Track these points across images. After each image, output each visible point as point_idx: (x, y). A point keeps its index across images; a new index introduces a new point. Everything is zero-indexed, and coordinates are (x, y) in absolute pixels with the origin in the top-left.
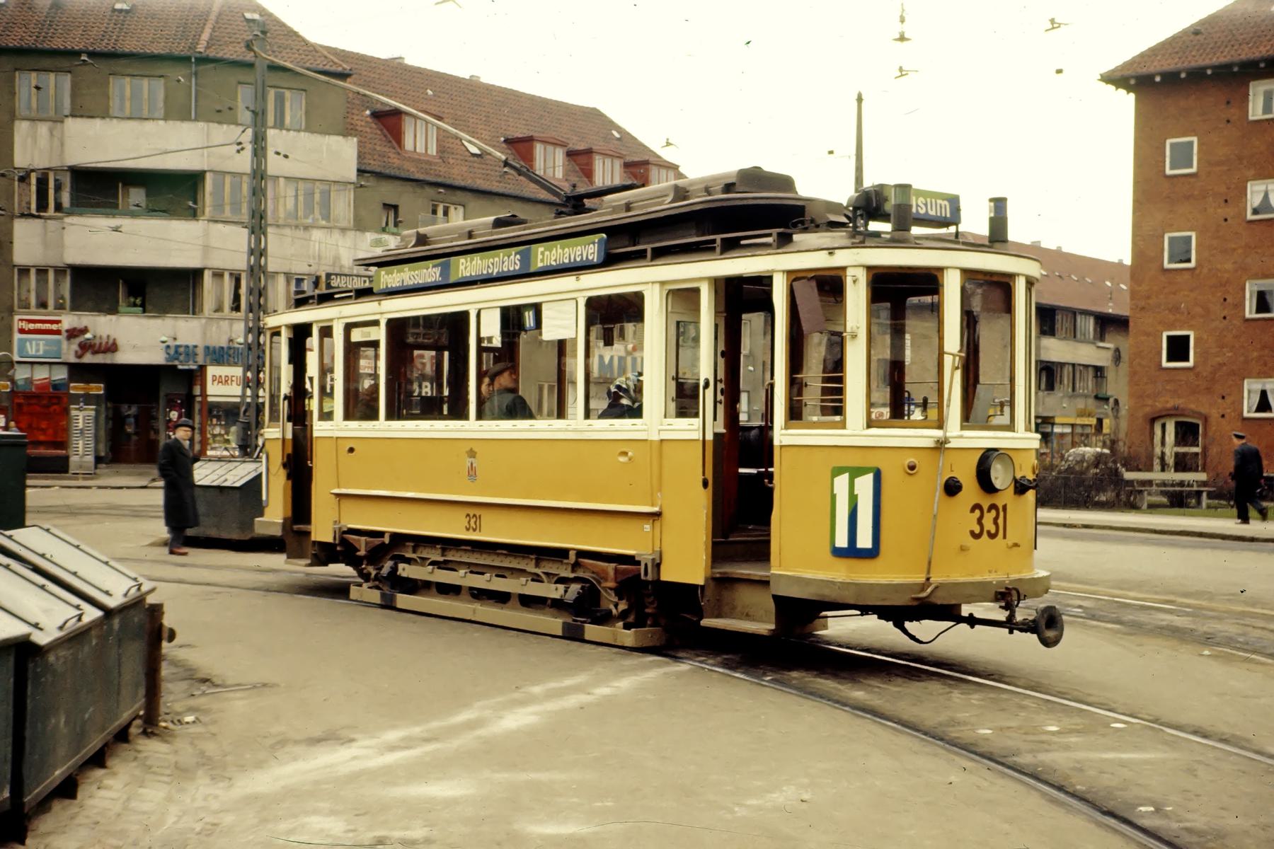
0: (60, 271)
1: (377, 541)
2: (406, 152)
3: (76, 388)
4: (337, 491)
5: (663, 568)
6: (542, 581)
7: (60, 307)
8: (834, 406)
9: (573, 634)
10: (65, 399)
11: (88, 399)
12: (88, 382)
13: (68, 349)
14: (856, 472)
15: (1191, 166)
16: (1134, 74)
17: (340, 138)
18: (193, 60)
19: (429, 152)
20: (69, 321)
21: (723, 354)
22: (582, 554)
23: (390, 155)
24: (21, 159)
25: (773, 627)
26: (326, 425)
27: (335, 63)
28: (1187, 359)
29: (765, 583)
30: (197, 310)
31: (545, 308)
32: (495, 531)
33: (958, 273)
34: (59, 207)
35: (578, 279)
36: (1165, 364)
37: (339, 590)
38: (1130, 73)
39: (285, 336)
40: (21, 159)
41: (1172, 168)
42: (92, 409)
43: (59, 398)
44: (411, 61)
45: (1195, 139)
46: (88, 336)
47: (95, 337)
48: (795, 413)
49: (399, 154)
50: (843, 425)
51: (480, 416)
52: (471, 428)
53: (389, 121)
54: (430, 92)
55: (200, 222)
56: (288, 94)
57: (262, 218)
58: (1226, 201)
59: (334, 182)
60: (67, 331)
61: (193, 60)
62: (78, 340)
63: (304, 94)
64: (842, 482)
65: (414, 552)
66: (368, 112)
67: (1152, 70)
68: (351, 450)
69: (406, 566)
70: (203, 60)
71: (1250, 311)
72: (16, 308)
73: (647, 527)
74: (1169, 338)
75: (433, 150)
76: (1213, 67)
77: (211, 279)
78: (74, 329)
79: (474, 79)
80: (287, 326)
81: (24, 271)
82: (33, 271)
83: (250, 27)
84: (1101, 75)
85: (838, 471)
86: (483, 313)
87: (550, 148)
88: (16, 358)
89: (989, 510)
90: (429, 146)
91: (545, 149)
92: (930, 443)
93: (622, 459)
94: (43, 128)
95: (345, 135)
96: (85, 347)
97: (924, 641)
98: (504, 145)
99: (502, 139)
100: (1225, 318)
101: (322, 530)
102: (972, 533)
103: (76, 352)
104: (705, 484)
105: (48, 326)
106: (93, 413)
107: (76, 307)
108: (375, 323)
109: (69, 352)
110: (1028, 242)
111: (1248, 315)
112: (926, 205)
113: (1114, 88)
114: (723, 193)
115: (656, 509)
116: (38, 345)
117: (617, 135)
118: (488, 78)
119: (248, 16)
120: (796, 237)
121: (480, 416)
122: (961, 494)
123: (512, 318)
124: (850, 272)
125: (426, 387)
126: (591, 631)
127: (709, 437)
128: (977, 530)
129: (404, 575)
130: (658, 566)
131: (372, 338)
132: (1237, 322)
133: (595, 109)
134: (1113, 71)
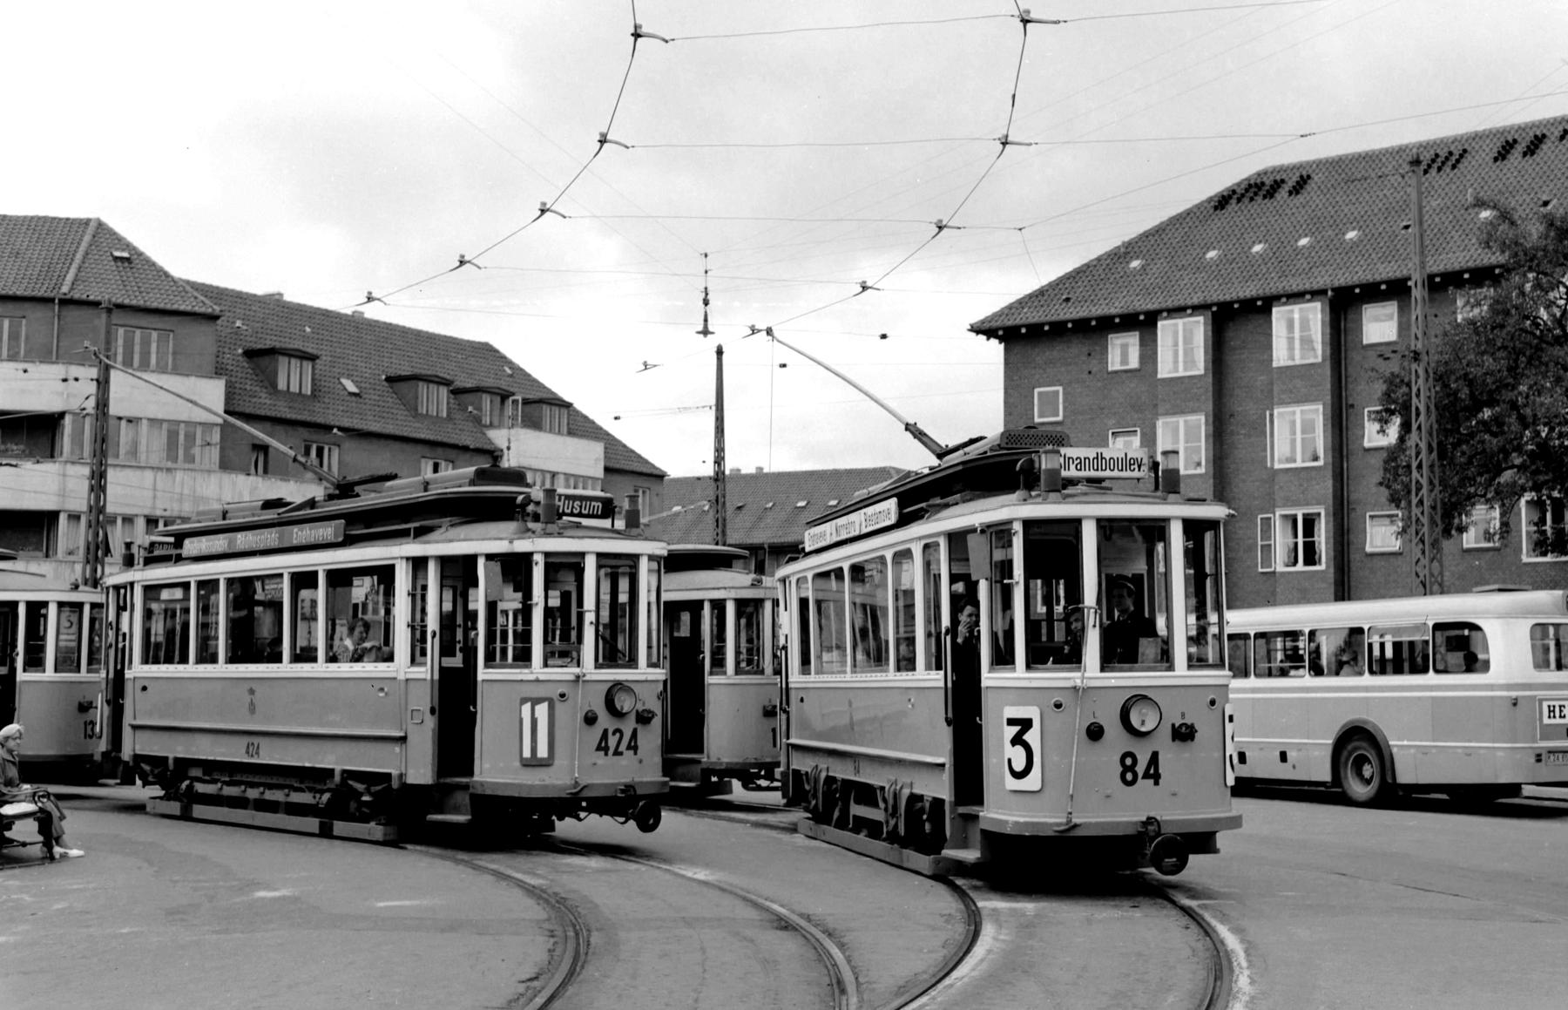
8: (524, 657)
9: (326, 833)
14: (536, 702)
18: (57, 301)
23: (261, 394)
25: (469, 817)
29: (466, 787)
30: (51, 553)
32: (271, 755)
38: (999, 324)
41: (1041, 416)
44: (292, 296)
45: (1060, 389)
48: (490, 659)
54: (308, 330)
55: (57, 464)
56: (155, 335)
61: (57, 301)
63: (171, 335)
64: (526, 708)
70: (66, 302)
73: (397, 749)
76: (1074, 321)
77: (66, 522)
85: (524, 701)
89: (614, 734)
92: (572, 678)
93: (382, 694)
98: (385, 383)
104: (433, 711)
112: (581, 507)
113: (984, 337)
114: (470, 485)
115: (402, 734)
119: (117, 254)
125: (1463, 453)
126: (339, 827)
129: (200, 791)
134: (983, 322)
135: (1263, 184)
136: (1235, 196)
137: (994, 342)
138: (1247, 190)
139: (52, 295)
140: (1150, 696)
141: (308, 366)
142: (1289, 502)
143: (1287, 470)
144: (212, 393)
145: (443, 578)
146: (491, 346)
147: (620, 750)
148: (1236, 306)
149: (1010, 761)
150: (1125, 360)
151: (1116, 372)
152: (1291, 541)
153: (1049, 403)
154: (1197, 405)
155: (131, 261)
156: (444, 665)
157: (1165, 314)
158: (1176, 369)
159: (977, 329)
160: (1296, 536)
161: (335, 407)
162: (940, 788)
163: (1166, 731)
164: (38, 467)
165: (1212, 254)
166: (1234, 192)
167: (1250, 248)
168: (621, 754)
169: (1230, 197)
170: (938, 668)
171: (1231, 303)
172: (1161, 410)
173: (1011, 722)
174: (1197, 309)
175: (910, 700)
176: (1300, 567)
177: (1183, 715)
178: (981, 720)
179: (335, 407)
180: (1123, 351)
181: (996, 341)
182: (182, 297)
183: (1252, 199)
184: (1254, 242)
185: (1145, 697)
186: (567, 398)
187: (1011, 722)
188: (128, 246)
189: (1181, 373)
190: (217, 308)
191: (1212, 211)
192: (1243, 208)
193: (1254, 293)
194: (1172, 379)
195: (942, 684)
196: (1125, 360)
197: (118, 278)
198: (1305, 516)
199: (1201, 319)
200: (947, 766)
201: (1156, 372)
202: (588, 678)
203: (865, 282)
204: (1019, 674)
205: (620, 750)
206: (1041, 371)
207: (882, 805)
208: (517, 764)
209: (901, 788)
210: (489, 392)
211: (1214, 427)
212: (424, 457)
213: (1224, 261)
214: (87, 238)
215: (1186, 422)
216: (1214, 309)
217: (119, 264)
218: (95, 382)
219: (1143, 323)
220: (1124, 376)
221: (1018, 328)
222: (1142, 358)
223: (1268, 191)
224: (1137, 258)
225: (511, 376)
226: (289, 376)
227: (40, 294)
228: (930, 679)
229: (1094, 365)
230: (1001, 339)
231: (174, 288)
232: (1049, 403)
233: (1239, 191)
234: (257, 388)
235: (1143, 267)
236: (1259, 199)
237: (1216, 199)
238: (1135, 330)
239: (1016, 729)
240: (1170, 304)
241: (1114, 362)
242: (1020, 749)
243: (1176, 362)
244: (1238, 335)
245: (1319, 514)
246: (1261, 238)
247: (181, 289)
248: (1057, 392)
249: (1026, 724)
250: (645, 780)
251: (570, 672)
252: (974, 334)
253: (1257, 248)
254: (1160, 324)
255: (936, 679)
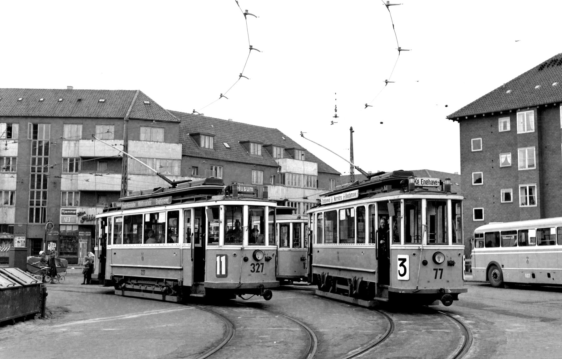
0: (77, 193)
1: (121, 278)
2: (202, 148)
3: (81, 234)
4: (111, 265)
5: (184, 282)
6: (158, 287)
7: (76, 205)
10: (77, 237)
11: (84, 237)
12: (85, 231)
13: (78, 220)
15: (480, 149)
16: (458, 116)
17: (176, 144)
19: (210, 148)
20: (79, 210)
21: (201, 226)
22: (166, 280)
24: (65, 154)
26: (109, 246)
27: (175, 118)
28: (482, 218)
31: (160, 214)
32: (148, 275)
33: (247, 206)
34: (77, 170)
35: (166, 207)
36: (474, 220)
37: (112, 293)
39: (100, 220)
40: (65, 154)
41: (474, 149)
42: (86, 241)
43: (75, 237)
45: (481, 139)
46: (85, 215)
47: (87, 215)
49: (199, 149)
50: (218, 244)
51: (115, 243)
52: (142, 246)
53: (196, 137)
54: (212, 126)
57: (125, 179)
58: (492, 161)
59: (174, 160)
60: (78, 213)
62: (81, 217)
64: (218, 258)
65: (130, 281)
66: (188, 134)
67: (464, 115)
68: (115, 254)
69: (128, 285)
71: (502, 200)
72: (61, 206)
74: (475, 210)
75: (212, 147)
78: (81, 213)
79: (230, 120)
80: (101, 218)
81: (64, 193)
82: (67, 193)
83: (146, 106)
84: (447, 117)
85: (217, 256)
86: (146, 215)
87: (256, 145)
88: (61, 223)
89: (256, 265)
90: (210, 145)
91: (254, 145)
92: (240, 249)
93: (175, 255)
94: (72, 143)
95: (177, 143)
96: (84, 219)
97: (245, 298)
99: (239, 142)
100: (494, 203)
101: (108, 277)
102: (251, 271)
103: (81, 221)
104: (192, 260)
105: (72, 212)
106: (87, 242)
107: (82, 205)
108: (121, 217)
109: (78, 221)
110: (453, 173)
111: (502, 202)
112: (246, 189)
113: (452, 121)
116: (68, 219)
117: (284, 138)
118: (235, 120)
119: (145, 102)
120: (212, 197)
121: (325, 242)
122: (535, 275)
123: (152, 216)
124: (221, 206)
127: (193, 248)
128: (253, 270)
130: (182, 282)
131: (121, 221)
132: (498, 204)
133: (276, 129)
134: (451, 115)
135: (557, 60)
136: (546, 65)
137: (456, 122)
138: (551, 63)
139: (123, 117)
140: (442, 252)
141: (211, 138)
142: (523, 182)
143: (523, 171)
144: (176, 150)
145: (196, 215)
146: (278, 130)
147: (259, 270)
148: (546, 106)
149: (399, 271)
150: (505, 127)
151: (502, 132)
152: (524, 196)
153: (477, 145)
154: (532, 143)
155: (151, 105)
156: (195, 246)
157: (519, 110)
158: (524, 130)
159: (449, 118)
160: (526, 194)
161: (221, 153)
162: (374, 279)
163: (446, 263)
164: (108, 175)
165: (537, 87)
166: (546, 63)
167: (552, 84)
168: (259, 272)
169: (545, 65)
170: (373, 242)
171: (544, 105)
172: (519, 145)
173: (400, 259)
174: (531, 108)
175: (363, 252)
176: (528, 205)
177: (451, 258)
178: (389, 258)
179: (221, 153)
180: (504, 124)
181: (457, 122)
182: (167, 116)
183: (553, 66)
184: (553, 82)
185: (440, 252)
186: (305, 148)
187: (400, 259)
188: (149, 99)
189: (526, 132)
190: (179, 119)
191: (538, 70)
192: (549, 69)
193: (553, 101)
194: (523, 134)
195: (375, 248)
196: (505, 127)
197: (146, 110)
198: (529, 187)
199: (533, 111)
200: (376, 273)
201: (516, 131)
202: (245, 249)
203: (367, 104)
204: (402, 245)
205: (259, 270)
206: (474, 132)
207: (349, 285)
208: (216, 277)
209: (358, 279)
210: (275, 146)
211: (539, 151)
212: (253, 170)
213: (542, 89)
214: (136, 97)
215: (528, 150)
216: (538, 107)
217: (146, 105)
218: (123, 146)
219: (511, 113)
220: (505, 133)
221: (464, 117)
222: (511, 126)
223: (559, 62)
224: (509, 89)
225: (284, 140)
226: (205, 142)
227: (119, 117)
228: (369, 246)
229: (493, 129)
230: (459, 121)
231: (165, 113)
232: (477, 145)
233: (548, 63)
234: (195, 147)
235: (511, 93)
236: (556, 66)
237: (540, 66)
238: (508, 116)
239: (401, 262)
240: (521, 106)
241: (501, 129)
242: (402, 268)
243: (524, 128)
244: (548, 116)
245: (534, 187)
246: (556, 80)
247: (167, 113)
248: (480, 140)
249: (404, 260)
250: (247, 282)
251: (237, 247)
252: (448, 120)
253: (554, 84)
254: (517, 113)
255: (373, 246)
